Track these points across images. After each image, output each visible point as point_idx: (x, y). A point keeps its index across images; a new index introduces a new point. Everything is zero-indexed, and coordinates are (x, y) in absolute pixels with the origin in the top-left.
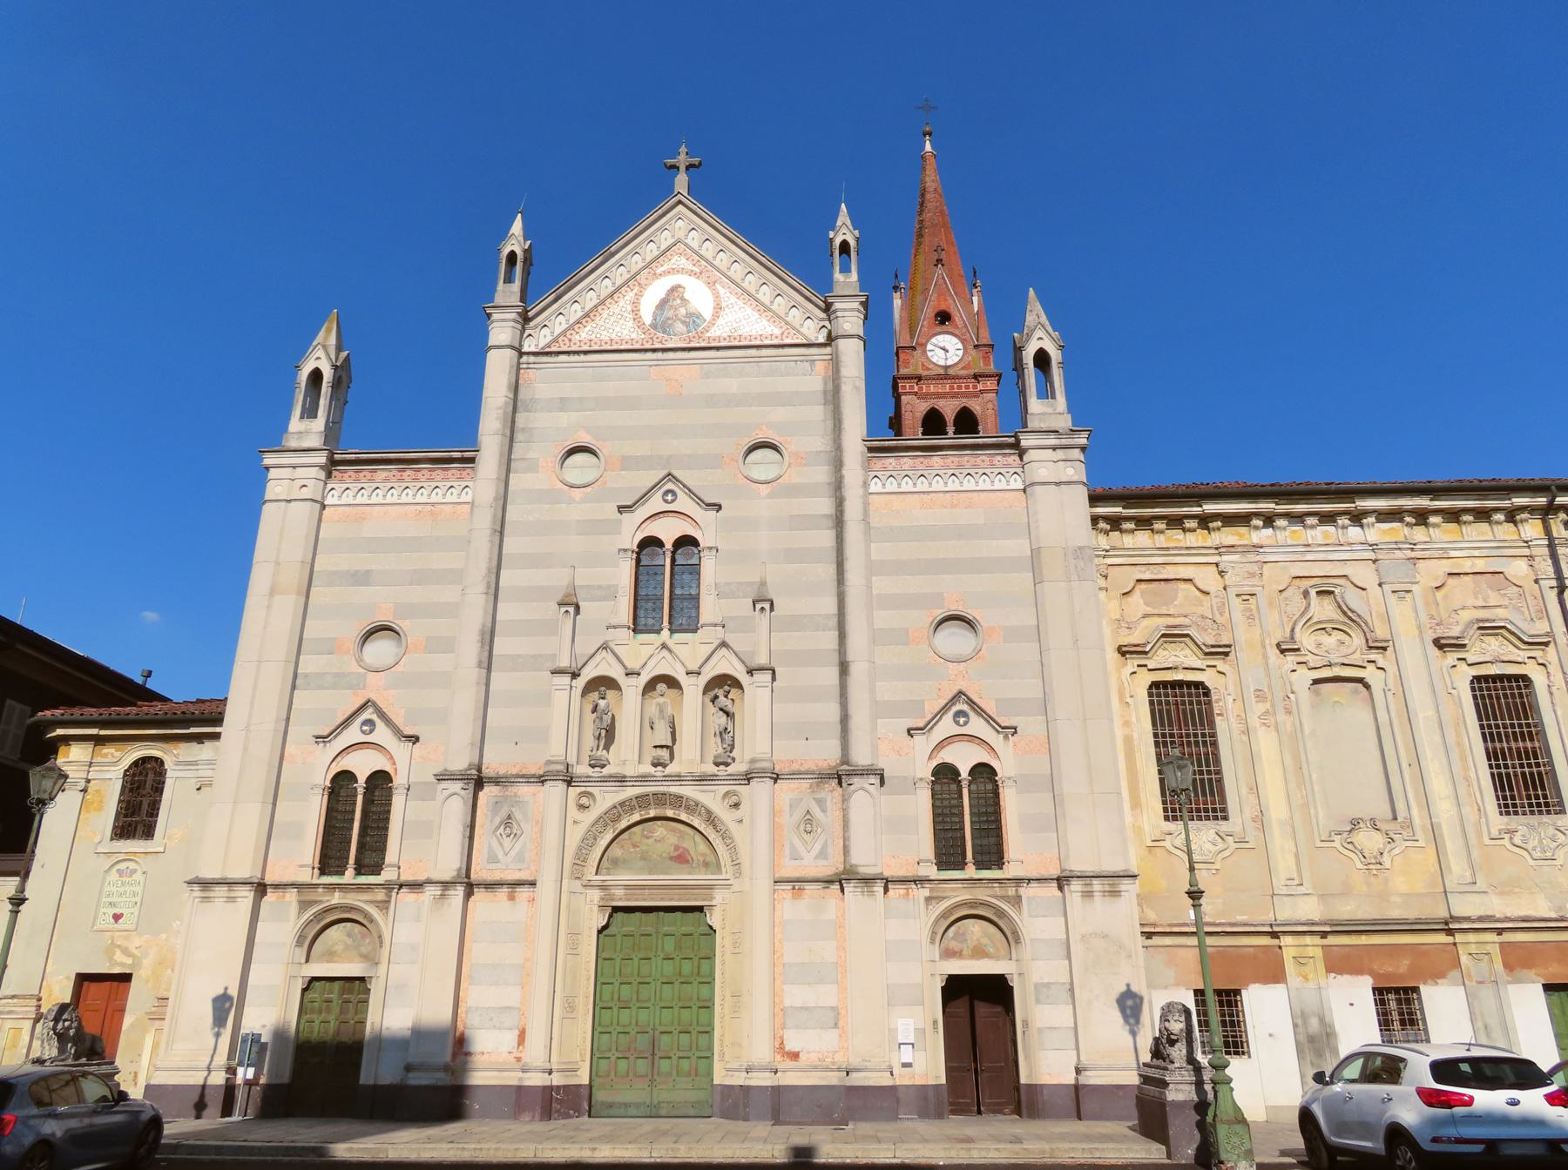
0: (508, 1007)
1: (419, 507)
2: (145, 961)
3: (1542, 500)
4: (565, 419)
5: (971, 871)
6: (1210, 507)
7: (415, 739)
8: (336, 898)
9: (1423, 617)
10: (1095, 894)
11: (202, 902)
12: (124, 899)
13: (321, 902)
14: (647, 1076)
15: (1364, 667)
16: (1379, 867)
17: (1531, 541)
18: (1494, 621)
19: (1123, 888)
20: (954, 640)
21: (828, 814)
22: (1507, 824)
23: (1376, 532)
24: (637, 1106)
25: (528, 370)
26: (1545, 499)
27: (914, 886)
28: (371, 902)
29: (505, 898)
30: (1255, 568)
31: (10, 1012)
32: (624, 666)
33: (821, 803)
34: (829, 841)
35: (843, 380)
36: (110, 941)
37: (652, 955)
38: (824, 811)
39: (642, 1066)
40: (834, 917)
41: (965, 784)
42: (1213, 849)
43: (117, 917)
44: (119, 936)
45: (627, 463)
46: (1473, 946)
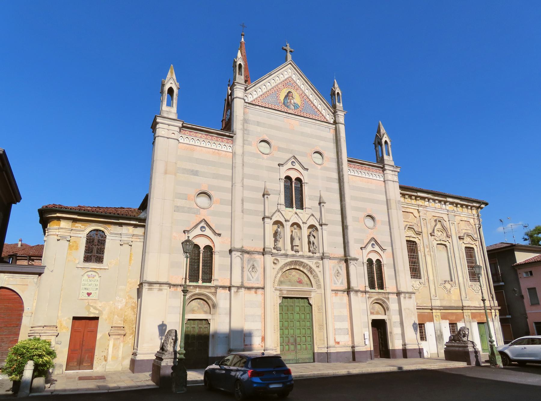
0: (257, 329)
1: (214, 150)
2: (104, 312)
3: (478, 205)
4: (259, 129)
5: (377, 290)
6: (419, 194)
7: (219, 235)
8: (197, 291)
9: (457, 231)
11: (148, 290)
12: (91, 287)
13: (192, 292)
14: (294, 350)
15: (446, 242)
16: (450, 293)
18: (469, 233)
19: (412, 296)
20: (203, 201)
21: (343, 270)
23: (449, 207)
24: (292, 360)
25: (246, 108)
26: (478, 205)
27: (180, 287)
28: (210, 293)
29: (254, 293)
30: (425, 212)
31: (45, 333)
32: (285, 218)
33: (340, 267)
34: (343, 279)
35: (341, 137)
36: (87, 304)
37: (293, 312)
38: (341, 270)
39: (292, 347)
40: (346, 302)
41: (201, 252)
42: (419, 286)
43: (89, 294)
44: (92, 302)
45: (279, 149)
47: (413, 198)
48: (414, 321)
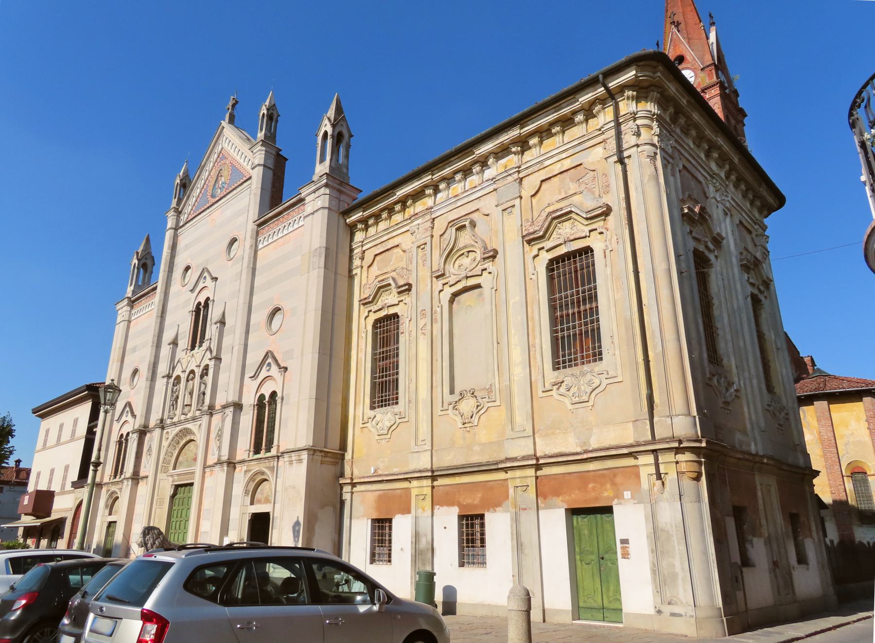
6: (401, 192)
10: (294, 462)
17: (602, 127)
22: (557, 377)
46: (518, 480)
47: (398, 207)
48: (298, 517)
